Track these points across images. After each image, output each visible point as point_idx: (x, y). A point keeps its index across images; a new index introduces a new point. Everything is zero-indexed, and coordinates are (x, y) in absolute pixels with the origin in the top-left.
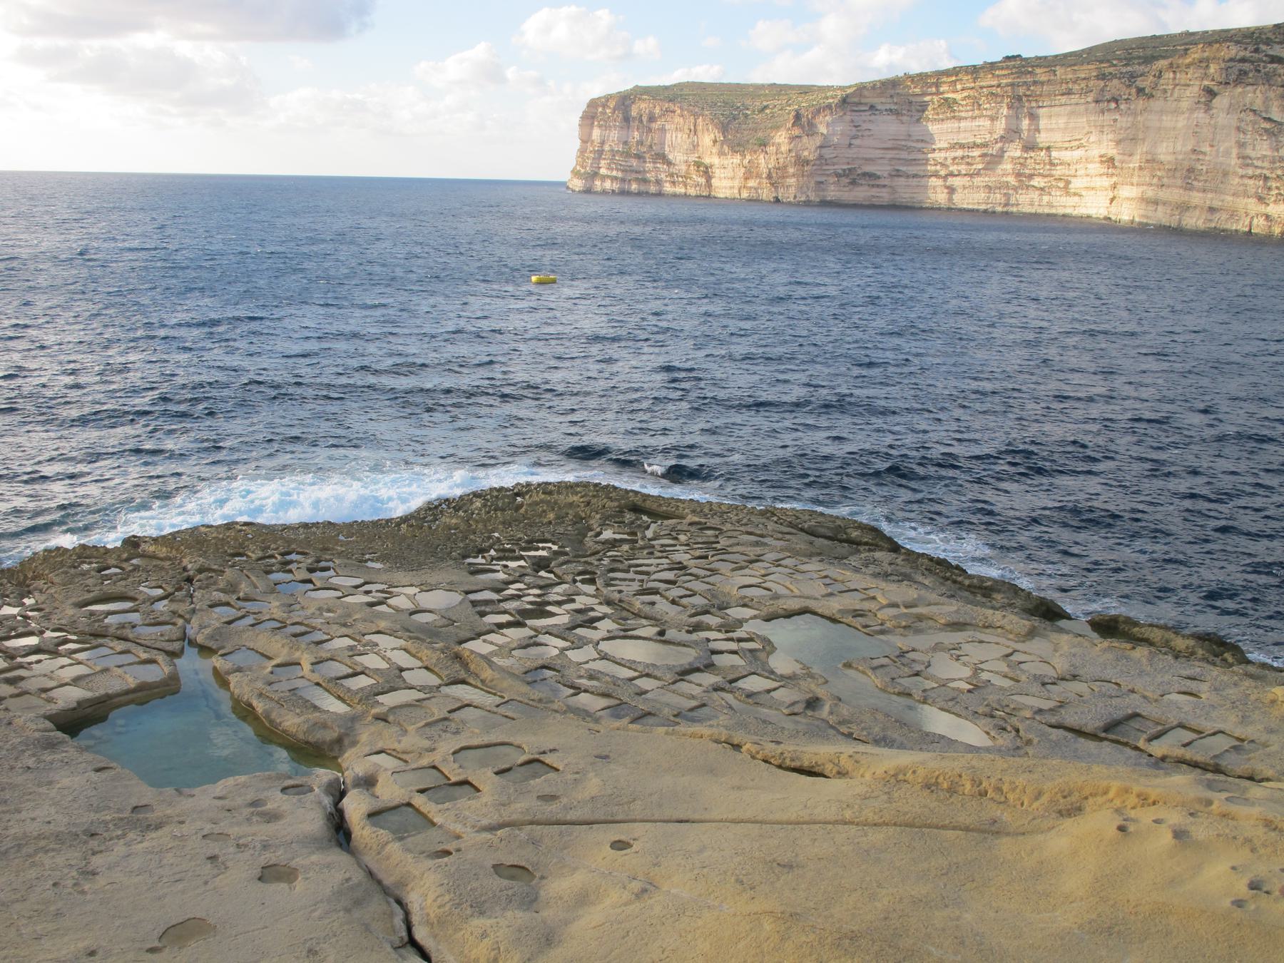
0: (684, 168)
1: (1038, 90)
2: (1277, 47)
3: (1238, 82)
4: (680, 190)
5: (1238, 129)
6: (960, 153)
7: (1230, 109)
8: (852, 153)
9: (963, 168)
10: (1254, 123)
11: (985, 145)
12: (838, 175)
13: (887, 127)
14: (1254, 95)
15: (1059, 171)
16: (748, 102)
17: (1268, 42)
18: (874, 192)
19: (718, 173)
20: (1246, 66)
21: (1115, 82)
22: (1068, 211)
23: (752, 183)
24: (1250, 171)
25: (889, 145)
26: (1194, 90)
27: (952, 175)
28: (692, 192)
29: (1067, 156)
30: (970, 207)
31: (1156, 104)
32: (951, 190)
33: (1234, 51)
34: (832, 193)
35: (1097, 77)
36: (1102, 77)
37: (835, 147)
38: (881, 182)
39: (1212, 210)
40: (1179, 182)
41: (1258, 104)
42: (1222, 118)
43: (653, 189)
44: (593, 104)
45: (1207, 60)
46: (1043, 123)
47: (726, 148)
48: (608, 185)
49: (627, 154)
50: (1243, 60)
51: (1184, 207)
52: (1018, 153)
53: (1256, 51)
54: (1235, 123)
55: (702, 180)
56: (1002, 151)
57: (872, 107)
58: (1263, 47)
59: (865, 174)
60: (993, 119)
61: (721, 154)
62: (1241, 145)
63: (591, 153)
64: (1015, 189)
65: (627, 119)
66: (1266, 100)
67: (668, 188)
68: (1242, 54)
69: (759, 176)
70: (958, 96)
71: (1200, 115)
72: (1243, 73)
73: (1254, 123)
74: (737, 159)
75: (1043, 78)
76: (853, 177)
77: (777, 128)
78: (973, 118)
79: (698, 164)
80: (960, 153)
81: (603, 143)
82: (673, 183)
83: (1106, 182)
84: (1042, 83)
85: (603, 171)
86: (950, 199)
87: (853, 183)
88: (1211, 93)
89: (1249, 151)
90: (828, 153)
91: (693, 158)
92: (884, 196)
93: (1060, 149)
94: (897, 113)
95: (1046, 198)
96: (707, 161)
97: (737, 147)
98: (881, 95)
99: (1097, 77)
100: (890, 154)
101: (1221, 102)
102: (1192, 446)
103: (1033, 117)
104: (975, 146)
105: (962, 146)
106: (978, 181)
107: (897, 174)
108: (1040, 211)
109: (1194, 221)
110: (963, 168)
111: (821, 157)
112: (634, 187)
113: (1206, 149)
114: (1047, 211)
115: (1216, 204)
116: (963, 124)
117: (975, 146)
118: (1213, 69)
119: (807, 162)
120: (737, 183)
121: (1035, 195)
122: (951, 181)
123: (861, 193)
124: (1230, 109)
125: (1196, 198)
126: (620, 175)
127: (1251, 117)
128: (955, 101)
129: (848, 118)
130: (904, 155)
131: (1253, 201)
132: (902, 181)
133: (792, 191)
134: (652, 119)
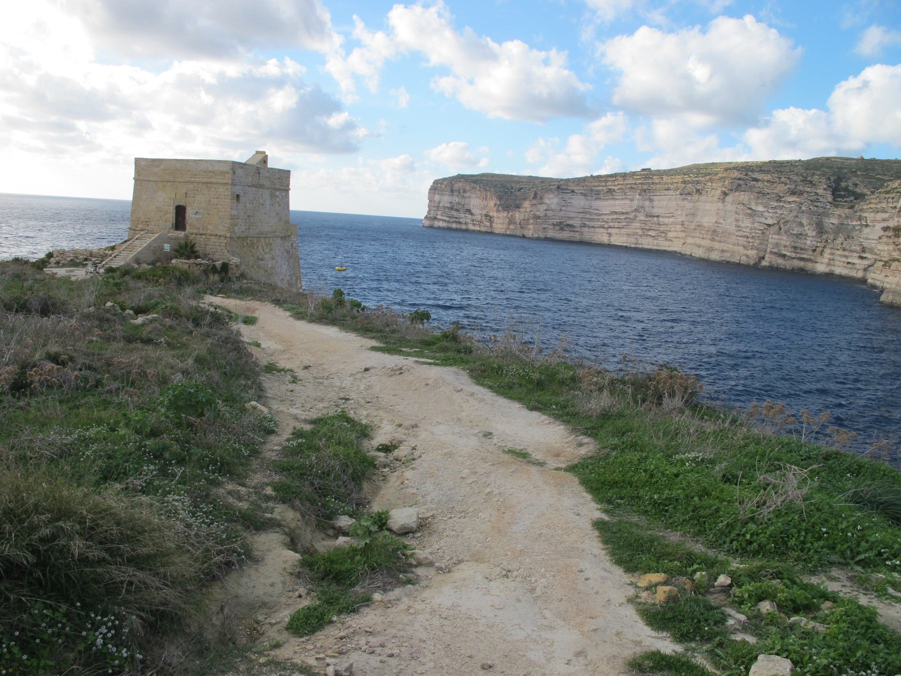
0: (479, 217)
1: (654, 187)
2: (756, 173)
3: (737, 190)
4: (477, 228)
5: (736, 212)
6: (615, 217)
7: (733, 203)
8: (562, 214)
9: (616, 225)
10: (743, 210)
11: (627, 213)
12: (554, 225)
13: (579, 202)
14: (743, 197)
15: (662, 228)
16: (513, 185)
17: (753, 171)
18: (572, 234)
19: (496, 220)
20: (741, 182)
21: (690, 185)
22: (666, 248)
23: (512, 227)
24: (740, 233)
25: (581, 210)
26: (718, 192)
27: (610, 227)
28: (483, 229)
29: (666, 220)
30: (649, 247)
31: (703, 198)
32: (610, 235)
33: (736, 174)
34: (551, 234)
35: (682, 182)
36: (684, 182)
37: (552, 210)
38: (576, 229)
39: (723, 251)
40: (709, 237)
41: (746, 201)
42: (730, 207)
43: (464, 227)
44: (436, 182)
45: (724, 178)
46: (656, 203)
47: (500, 208)
48: (441, 224)
49: (452, 209)
50: (740, 179)
51: (711, 249)
52: (643, 218)
53: (746, 175)
54: (734, 209)
55: (488, 224)
56: (636, 216)
57: (573, 191)
58: (749, 173)
59: (568, 225)
60: (632, 200)
61: (498, 211)
62: (737, 220)
63: (433, 206)
64: (641, 236)
65: (452, 191)
66: (750, 199)
67: (471, 227)
68: (739, 176)
69: (515, 223)
70: (615, 188)
71: (720, 205)
72: (739, 185)
73: (743, 210)
74: (505, 214)
75: (657, 181)
76: (561, 226)
77: (525, 199)
78: (622, 199)
79: (486, 216)
80: (615, 217)
81: (439, 202)
82: (474, 225)
83: (683, 235)
84: (656, 184)
85: (439, 217)
86: (491, 226)
87: (562, 229)
88: (725, 194)
89: (740, 224)
90: (549, 213)
91: (484, 212)
92: (577, 237)
93: (664, 217)
94: (585, 195)
95: (656, 242)
96: (491, 214)
97: (506, 208)
98: (578, 185)
99: (682, 182)
100: (581, 215)
101: (729, 199)
102: (439, 273)
103: (651, 200)
104: (623, 213)
105: (616, 213)
106: (623, 231)
107: (584, 226)
108: (653, 247)
109: (715, 256)
110: (616, 225)
111: (546, 215)
112: (454, 226)
113: (722, 221)
114: (656, 248)
115: (725, 248)
116: (617, 202)
117: (623, 213)
118: (727, 182)
119: (539, 217)
120: (505, 226)
121: (650, 240)
122: (610, 230)
123: (566, 235)
124: (733, 203)
125: (717, 245)
126: (447, 219)
127: (742, 207)
128: (614, 191)
129: (560, 196)
130: (588, 216)
131: (741, 248)
132: (586, 229)
133: (531, 232)
134: (465, 191)
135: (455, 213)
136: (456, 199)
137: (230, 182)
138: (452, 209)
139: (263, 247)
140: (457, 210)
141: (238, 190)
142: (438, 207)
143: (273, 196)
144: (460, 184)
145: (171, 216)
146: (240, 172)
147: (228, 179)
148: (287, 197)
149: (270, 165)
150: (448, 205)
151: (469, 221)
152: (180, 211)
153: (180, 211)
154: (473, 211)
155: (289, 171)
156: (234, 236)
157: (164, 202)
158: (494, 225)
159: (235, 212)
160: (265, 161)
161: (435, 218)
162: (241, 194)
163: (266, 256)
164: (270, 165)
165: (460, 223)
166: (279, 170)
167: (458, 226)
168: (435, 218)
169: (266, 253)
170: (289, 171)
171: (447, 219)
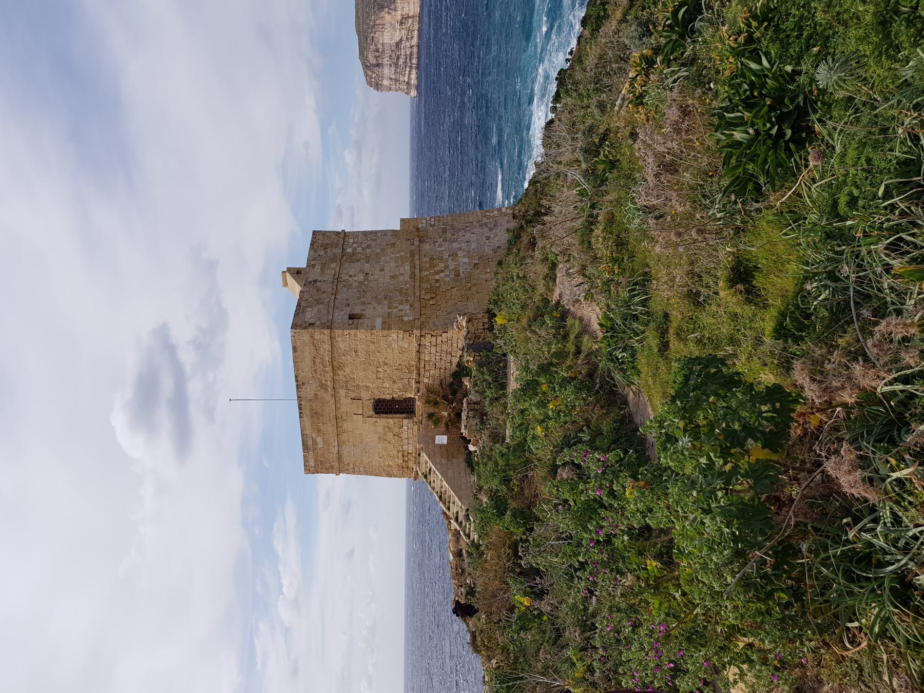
28: (416, 27)
43: (415, 50)
44: (370, 84)
48: (414, 76)
55: (410, 21)
61: (395, 10)
79: (401, 23)
81: (391, 79)
91: (398, 26)
96: (399, 18)
112: (414, 61)
126: (408, 69)
134: (377, 51)
135: (401, 61)
136: (386, 61)
137: (327, 331)
138: (396, 65)
139: (436, 273)
140: (398, 58)
141: (341, 316)
142: (396, 80)
143: (353, 258)
144: (370, 56)
145: (391, 421)
146: (309, 316)
147: (322, 336)
148: (355, 234)
149: (303, 264)
150: (393, 69)
151: (408, 44)
152: (383, 407)
153: (383, 407)
154: (397, 40)
155: (314, 233)
156: (418, 323)
157: (370, 431)
158: (410, 14)
159: (379, 322)
160: (296, 273)
161: (408, 83)
162: (348, 310)
163: (452, 267)
164: (303, 264)
165: (411, 54)
166: (365, 233)
167: (415, 56)
168: (408, 83)
169: (447, 267)
170: (314, 233)
171: (408, 69)
